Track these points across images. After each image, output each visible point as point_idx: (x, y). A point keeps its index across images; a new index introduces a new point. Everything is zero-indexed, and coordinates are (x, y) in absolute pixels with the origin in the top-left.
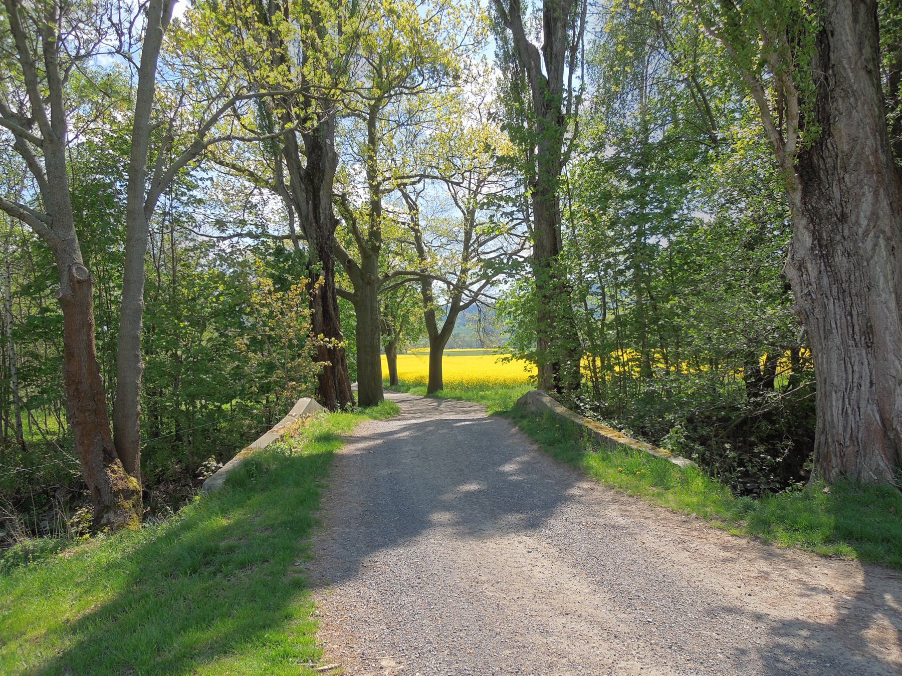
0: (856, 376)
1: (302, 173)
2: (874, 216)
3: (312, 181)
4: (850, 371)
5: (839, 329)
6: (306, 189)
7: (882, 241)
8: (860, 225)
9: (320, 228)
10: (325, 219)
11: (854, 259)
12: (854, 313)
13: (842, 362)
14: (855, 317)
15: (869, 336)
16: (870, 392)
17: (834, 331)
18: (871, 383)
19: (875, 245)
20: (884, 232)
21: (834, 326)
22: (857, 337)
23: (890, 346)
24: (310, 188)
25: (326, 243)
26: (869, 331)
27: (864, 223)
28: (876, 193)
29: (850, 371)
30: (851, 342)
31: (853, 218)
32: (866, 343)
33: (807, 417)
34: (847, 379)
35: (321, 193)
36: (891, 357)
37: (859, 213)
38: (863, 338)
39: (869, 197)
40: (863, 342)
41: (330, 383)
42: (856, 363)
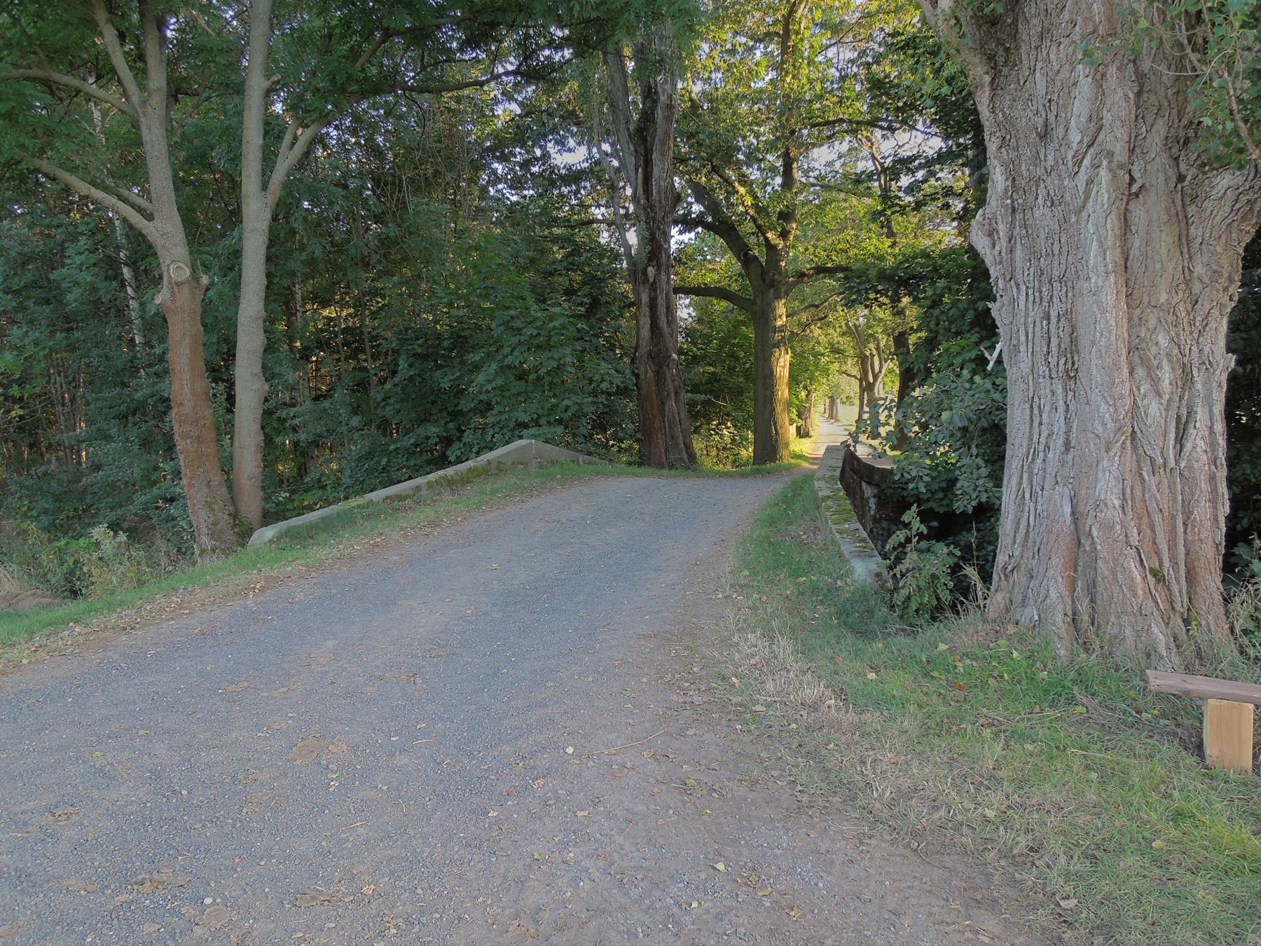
0: (1045, 434)
1: (631, 128)
2: (1096, 123)
3: (645, 140)
4: (1036, 424)
5: (1030, 345)
6: (636, 151)
7: (1104, 173)
8: (1069, 146)
9: (652, 207)
10: (659, 193)
11: (1058, 211)
12: (1053, 314)
13: (1027, 406)
14: (1054, 320)
15: (112, 509)
16: (1063, 463)
17: (1023, 348)
18: (1067, 444)
19: (1090, 182)
20: (1110, 154)
21: (1023, 339)
22: (1053, 361)
23: (1098, 377)
24: (641, 149)
25: (658, 228)
26: (1072, 349)
27: (1075, 137)
28: (1099, 79)
29: (1036, 424)
30: (1042, 369)
31: (1060, 131)
32: (1067, 371)
33: (1237, 457)
34: (1031, 435)
35: (654, 156)
36: (1095, 397)
37: (1068, 122)
38: (1062, 361)
39: (1085, 86)
40: (1061, 368)
41: (657, 424)
42: (1047, 408)
